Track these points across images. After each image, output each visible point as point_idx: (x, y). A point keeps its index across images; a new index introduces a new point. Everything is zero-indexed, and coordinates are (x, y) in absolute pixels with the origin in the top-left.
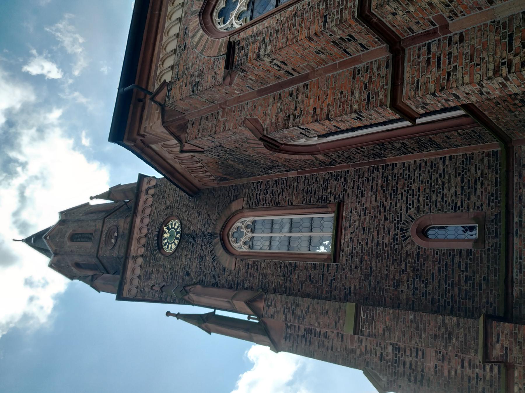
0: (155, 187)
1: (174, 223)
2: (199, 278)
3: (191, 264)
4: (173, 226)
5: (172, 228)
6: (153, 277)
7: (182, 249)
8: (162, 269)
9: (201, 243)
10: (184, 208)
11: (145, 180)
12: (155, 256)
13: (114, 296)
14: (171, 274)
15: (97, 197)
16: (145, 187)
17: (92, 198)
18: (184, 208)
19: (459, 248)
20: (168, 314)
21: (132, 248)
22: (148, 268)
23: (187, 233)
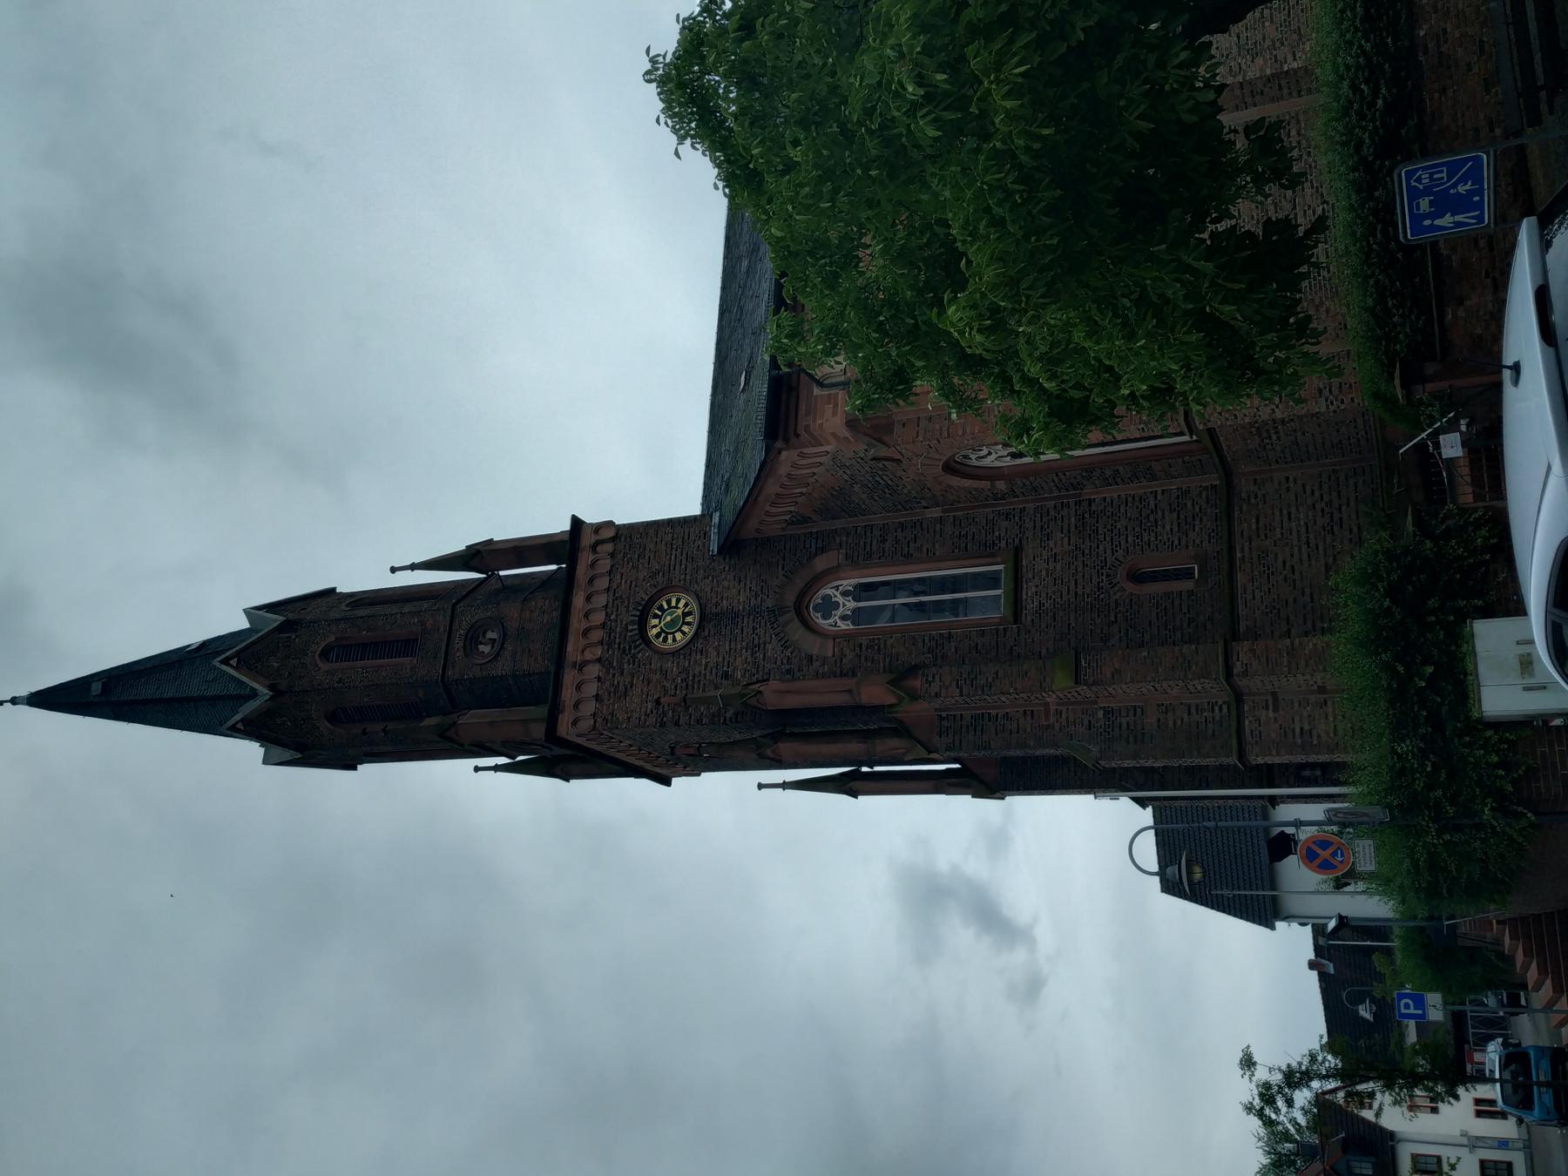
15: (413, 567)
17: (393, 570)
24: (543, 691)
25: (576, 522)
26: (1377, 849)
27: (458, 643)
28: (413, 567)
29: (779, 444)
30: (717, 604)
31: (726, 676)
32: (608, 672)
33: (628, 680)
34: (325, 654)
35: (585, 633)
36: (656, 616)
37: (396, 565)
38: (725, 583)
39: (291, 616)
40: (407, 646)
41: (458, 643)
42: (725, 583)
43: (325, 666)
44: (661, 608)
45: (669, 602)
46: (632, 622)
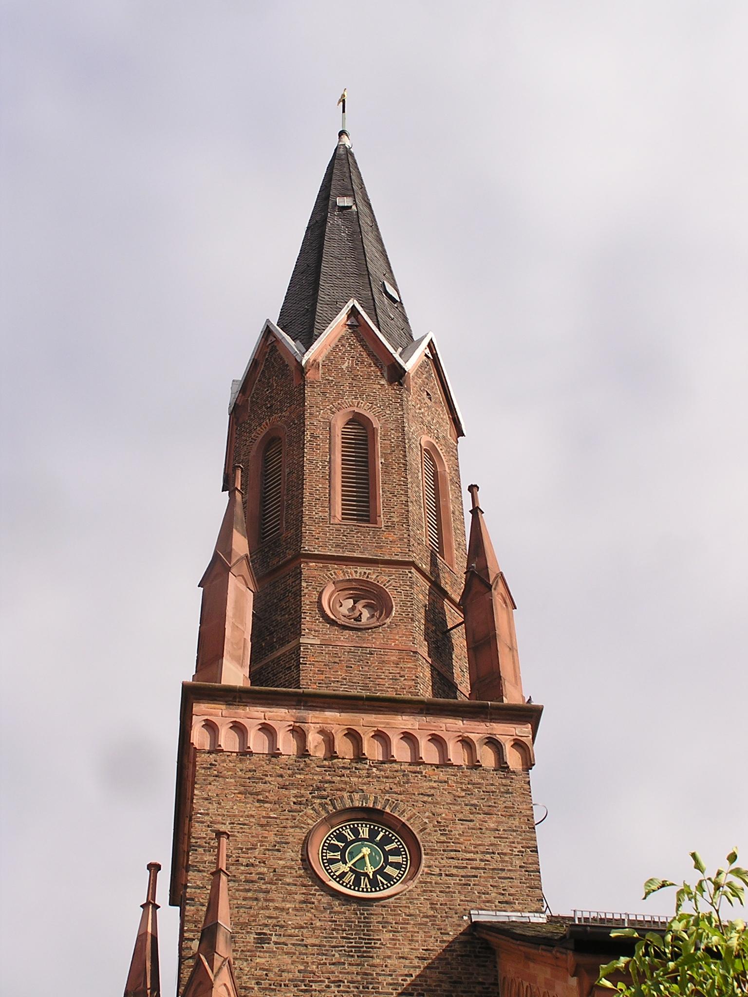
0: (502, 765)
1: (394, 845)
2: (252, 984)
3: (290, 948)
4: (391, 859)
5: (386, 854)
6: (252, 808)
7: (330, 906)
8: (272, 838)
9: (346, 978)
10: (443, 899)
11: (523, 731)
12: (308, 803)
13: (189, 679)
14: (261, 877)
15: (476, 511)
16: (506, 732)
17: (473, 488)
18: (443, 899)
19: (340, 509)
20: (154, 868)
21: (328, 714)
22: (275, 782)
23: (374, 919)
24: (276, 675)
25: (530, 715)
26: (298, 538)
27: (357, 572)
28: (476, 511)
29: (570, 958)
30: (385, 923)
31: (262, 939)
32: (286, 767)
33: (272, 797)
34: (358, 421)
35: (493, 742)
36: (373, 834)
37: (480, 494)
38: (420, 936)
39: (414, 383)
40: (362, 506)
41: (357, 572)
42: (420, 936)
43: (339, 423)
44: (387, 840)
45: (396, 852)
46: (365, 798)
